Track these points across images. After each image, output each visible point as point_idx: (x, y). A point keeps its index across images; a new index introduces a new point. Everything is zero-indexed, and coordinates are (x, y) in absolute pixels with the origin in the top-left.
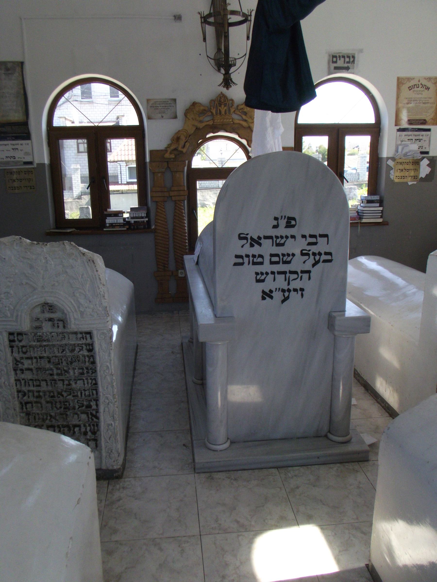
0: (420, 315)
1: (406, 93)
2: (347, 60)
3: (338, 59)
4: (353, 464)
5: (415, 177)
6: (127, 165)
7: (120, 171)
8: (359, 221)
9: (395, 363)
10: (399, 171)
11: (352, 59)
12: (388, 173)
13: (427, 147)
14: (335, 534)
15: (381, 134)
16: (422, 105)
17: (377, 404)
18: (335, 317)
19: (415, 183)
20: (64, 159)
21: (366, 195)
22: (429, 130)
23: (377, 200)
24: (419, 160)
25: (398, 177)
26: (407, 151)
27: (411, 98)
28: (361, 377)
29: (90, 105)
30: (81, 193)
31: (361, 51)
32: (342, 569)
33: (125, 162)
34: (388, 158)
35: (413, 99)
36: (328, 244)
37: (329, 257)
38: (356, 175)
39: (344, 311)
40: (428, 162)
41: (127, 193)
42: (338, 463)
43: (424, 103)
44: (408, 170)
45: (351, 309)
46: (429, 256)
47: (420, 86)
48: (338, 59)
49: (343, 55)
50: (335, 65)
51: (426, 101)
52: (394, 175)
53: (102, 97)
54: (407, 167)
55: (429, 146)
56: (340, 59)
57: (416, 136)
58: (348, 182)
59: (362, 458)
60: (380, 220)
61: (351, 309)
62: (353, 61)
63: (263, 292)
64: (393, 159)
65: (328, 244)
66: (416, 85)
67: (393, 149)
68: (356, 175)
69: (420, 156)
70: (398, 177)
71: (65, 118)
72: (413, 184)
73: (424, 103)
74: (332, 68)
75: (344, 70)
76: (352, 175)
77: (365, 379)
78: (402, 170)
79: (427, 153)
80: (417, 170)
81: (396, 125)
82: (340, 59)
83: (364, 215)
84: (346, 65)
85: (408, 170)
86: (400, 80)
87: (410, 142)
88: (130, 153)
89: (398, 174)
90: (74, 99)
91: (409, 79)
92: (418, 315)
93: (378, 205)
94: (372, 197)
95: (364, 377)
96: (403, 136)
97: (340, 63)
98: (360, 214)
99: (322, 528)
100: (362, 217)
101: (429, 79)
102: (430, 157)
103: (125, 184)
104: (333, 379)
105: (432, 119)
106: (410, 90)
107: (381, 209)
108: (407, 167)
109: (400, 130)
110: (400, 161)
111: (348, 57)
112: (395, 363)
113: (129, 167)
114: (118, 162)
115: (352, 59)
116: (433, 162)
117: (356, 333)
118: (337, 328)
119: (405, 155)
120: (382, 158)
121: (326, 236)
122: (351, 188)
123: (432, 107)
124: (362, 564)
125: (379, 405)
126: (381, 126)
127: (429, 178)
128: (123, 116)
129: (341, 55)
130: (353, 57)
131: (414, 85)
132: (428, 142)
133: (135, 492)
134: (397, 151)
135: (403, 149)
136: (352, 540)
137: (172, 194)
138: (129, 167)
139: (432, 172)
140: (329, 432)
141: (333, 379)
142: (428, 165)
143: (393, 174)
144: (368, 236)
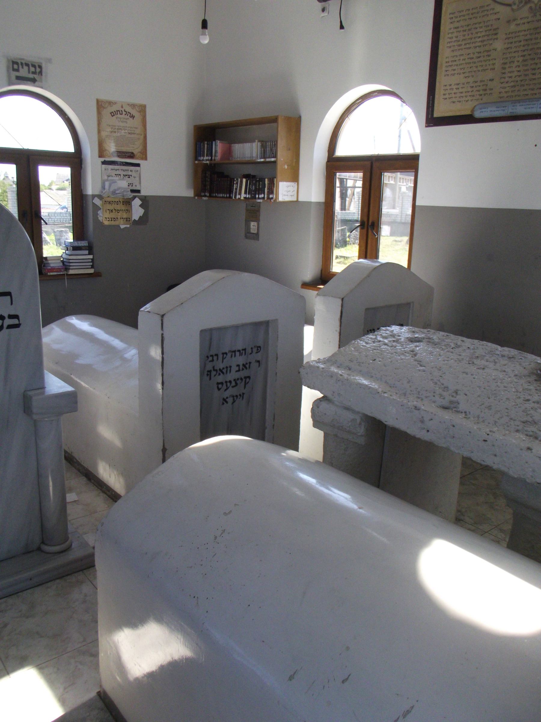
0: (137, 382)
2: (32, 69)
3: (20, 66)
4: (76, 574)
5: (128, 220)
8: (65, 273)
9: (117, 443)
10: (108, 211)
11: (38, 70)
12: (96, 215)
14: (58, 669)
15: (83, 166)
17: (102, 494)
18: (31, 397)
19: (128, 226)
21: (72, 241)
22: (138, 165)
23: (85, 246)
24: (130, 199)
25: (108, 219)
26: (116, 188)
27: (115, 126)
28: (82, 466)
31: (49, 61)
32: (69, 710)
34: (94, 196)
35: (117, 127)
36: (12, 304)
37: (15, 321)
38: (67, 215)
39: (43, 388)
40: (140, 202)
42: (57, 579)
43: (129, 133)
44: (118, 211)
45: (55, 385)
46: (140, 313)
47: (124, 113)
48: (20, 66)
50: (17, 74)
52: (104, 217)
54: (119, 207)
55: (140, 183)
56: (23, 68)
57: (124, 170)
58: (46, 224)
59: (87, 565)
60: (92, 271)
61: (55, 385)
62: (41, 73)
64: (100, 197)
65: (12, 304)
67: (99, 185)
68: (67, 215)
69: (131, 195)
70: (108, 219)
72: (126, 228)
73: (129, 133)
74: (13, 78)
75: (29, 82)
76: (62, 215)
77: (86, 466)
78: (112, 211)
79: (139, 191)
80: (129, 211)
81: (100, 157)
82: (23, 68)
83: (71, 264)
84: (31, 76)
85: (118, 211)
87: (117, 178)
89: (107, 215)
91: (110, 103)
92: (134, 382)
93: (87, 252)
94: (79, 242)
95: (84, 465)
96: (110, 170)
97: (24, 72)
98: (65, 263)
99: (40, 668)
100: (68, 267)
101: (133, 106)
104: (39, 476)
105: (140, 152)
106: (112, 116)
107: (91, 257)
108: (119, 207)
109: (104, 163)
110: (109, 199)
111: (34, 66)
112: (117, 443)
115: (38, 70)
116: (146, 202)
117: (60, 414)
118: (34, 410)
119: (114, 193)
120: (87, 195)
121: (9, 294)
122: (61, 231)
123: (139, 139)
124: (93, 694)
125: (105, 495)
126: (82, 157)
127: (143, 220)
129: (24, 62)
130: (40, 67)
132: (137, 179)
133: (21, 611)
134: (103, 187)
135: (110, 186)
136: (79, 669)
139: (145, 214)
140: (43, 543)
141: (39, 476)
142: (140, 206)
143: (101, 215)
144: (65, 291)
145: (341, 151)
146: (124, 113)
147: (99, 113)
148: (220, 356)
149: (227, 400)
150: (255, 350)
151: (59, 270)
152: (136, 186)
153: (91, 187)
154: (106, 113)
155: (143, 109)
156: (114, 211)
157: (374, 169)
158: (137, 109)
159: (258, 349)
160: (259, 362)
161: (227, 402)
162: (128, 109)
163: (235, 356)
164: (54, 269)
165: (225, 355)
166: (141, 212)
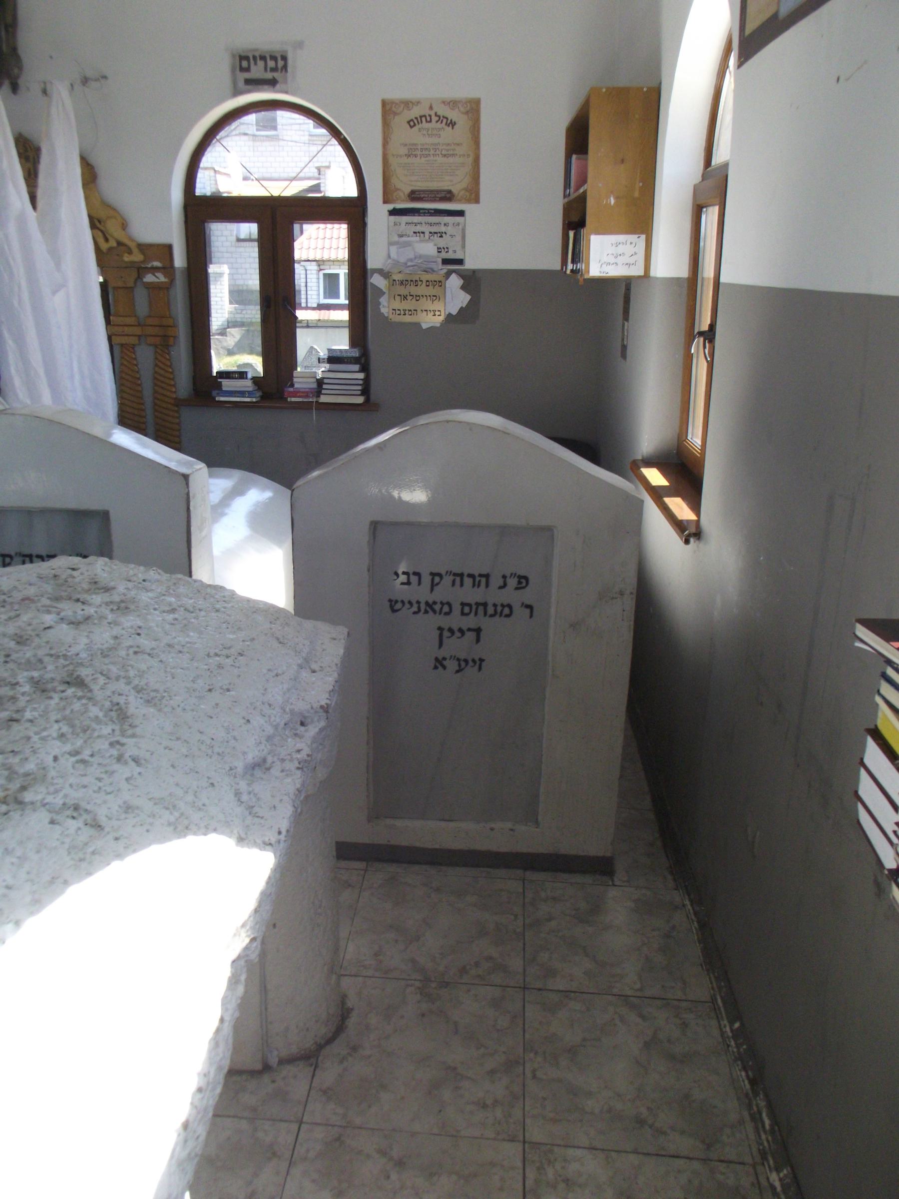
1: (402, 134)
2: (271, 64)
3: (252, 62)
6: (321, 270)
7: (304, 280)
10: (398, 298)
13: (458, 248)
16: (440, 159)
20: (211, 252)
22: (461, 213)
25: (398, 312)
27: (415, 145)
29: (272, 143)
30: (228, 322)
31: (300, 45)
33: (314, 263)
35: (419, 147)
41: (316, 327)
47: (434, 119)
48: (252, 62)
49: (263, 54)
50: (247, 75)
51: (448, 150)
53: (297, 127)
55: (463, 246)
56: (256, 64)
57: (431, 224)
62: (285, 67)
63: (437, 659)
66: (425, 116)
71: (215, 171)
74: (241, 84)
75: (266, 87)
79: (460, 262)
81: (385, 202)
82: (256, 64)
84: (269, 75)
86: (388, 107)
88: (334, 243)
90: (242, 131)
91: (408, 104)
97: (258, 71)
101: (453, 104)
102: (467, 270)
103: (314, 309)
105: (466, 189)
106: (411, 127)
109: (394, 212)
111: (273, 58)
113: (324, 275)
114: (302, 263)
115: (281, 63)
128: (328, 167)
129: (257, 54)
130: (284, 58)
131: (421, 117)
132: (458, 238)
137: (138, 331)
138: (324, 275)
139: (474, 304)
143: (386, 304)
145: (204, 186)
146: (434, 119)
147: (386, 124)
148: (426, 580)
149: (445, 663)
150: (512, 582)
151: (306, 394)
152: (455, 252)
153: (375, 258)
154: (399, 122)
155: (473, 108)
156: (409, 298)
157: (275, 220)
158: (462, 109)
159: (519, 583)
160: (530, 607)
161: (444, 667)
162: (443, 111)
163: (462, 585)
164: (299, 392)
165: (437, 579)
166: (463, 299)
